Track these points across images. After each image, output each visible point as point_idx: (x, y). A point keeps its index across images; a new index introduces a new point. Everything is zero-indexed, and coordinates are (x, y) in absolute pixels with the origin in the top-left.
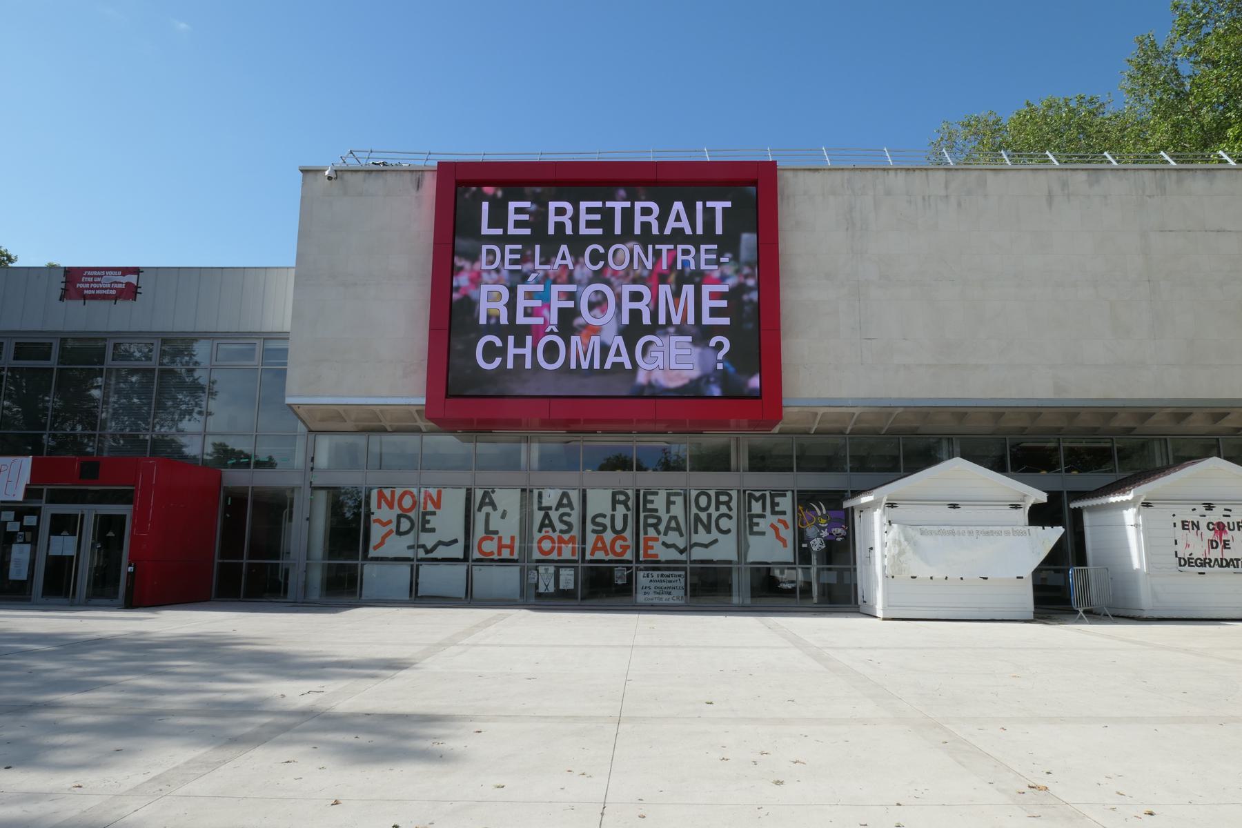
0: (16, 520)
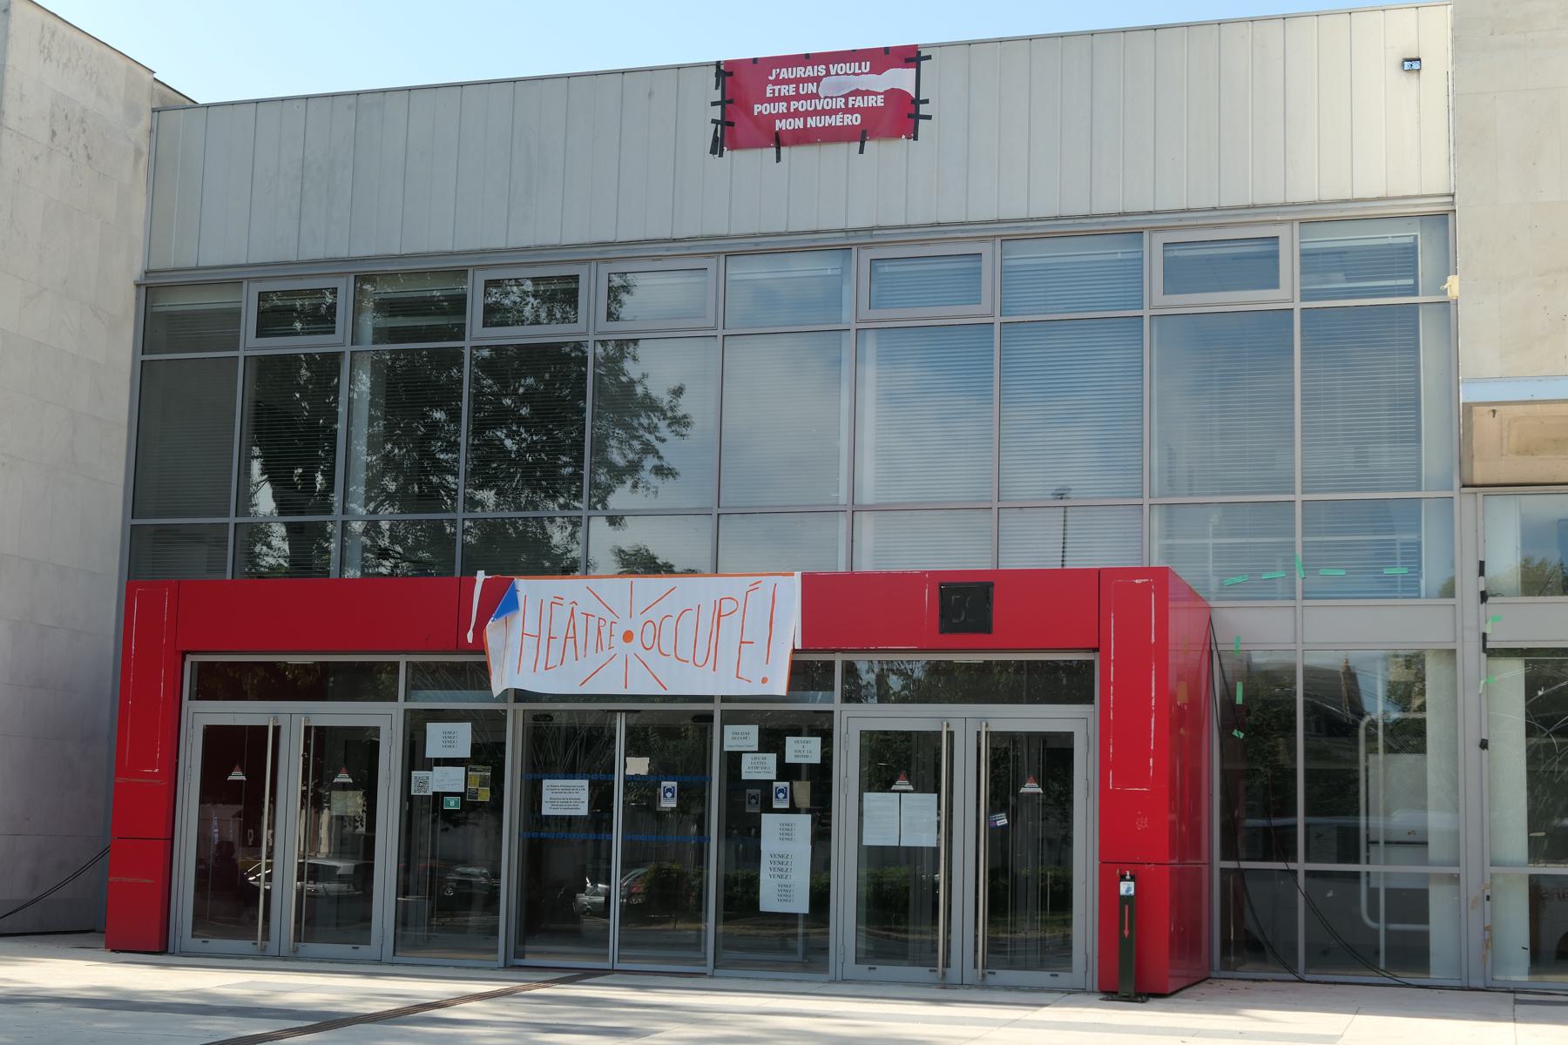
0: (764, 747)
